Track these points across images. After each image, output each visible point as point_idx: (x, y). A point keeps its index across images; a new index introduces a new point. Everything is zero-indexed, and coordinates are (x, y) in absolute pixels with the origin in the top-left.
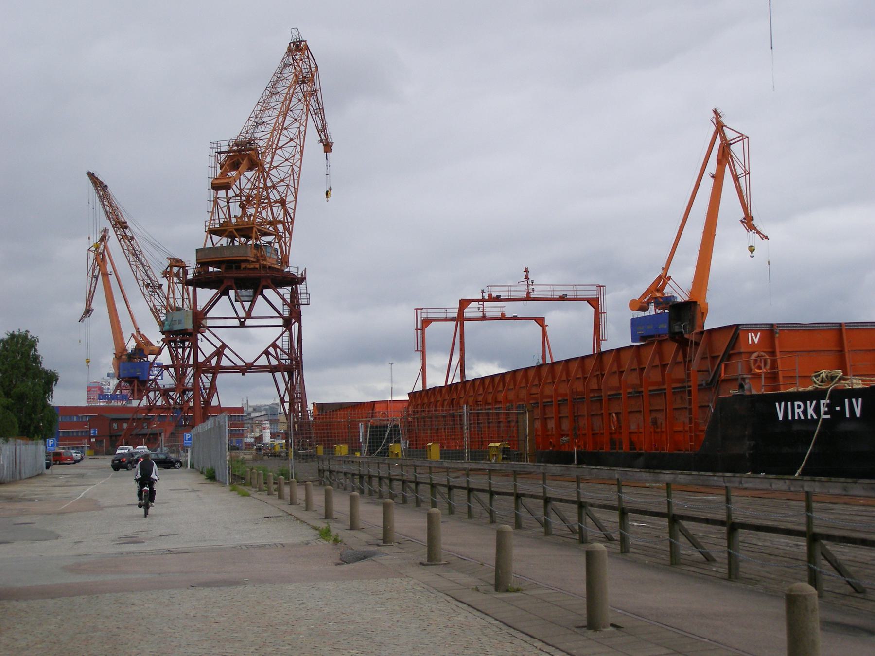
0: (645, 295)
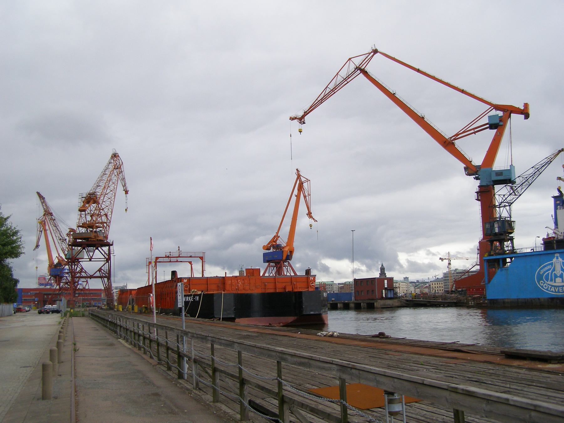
0: (269, 244)
